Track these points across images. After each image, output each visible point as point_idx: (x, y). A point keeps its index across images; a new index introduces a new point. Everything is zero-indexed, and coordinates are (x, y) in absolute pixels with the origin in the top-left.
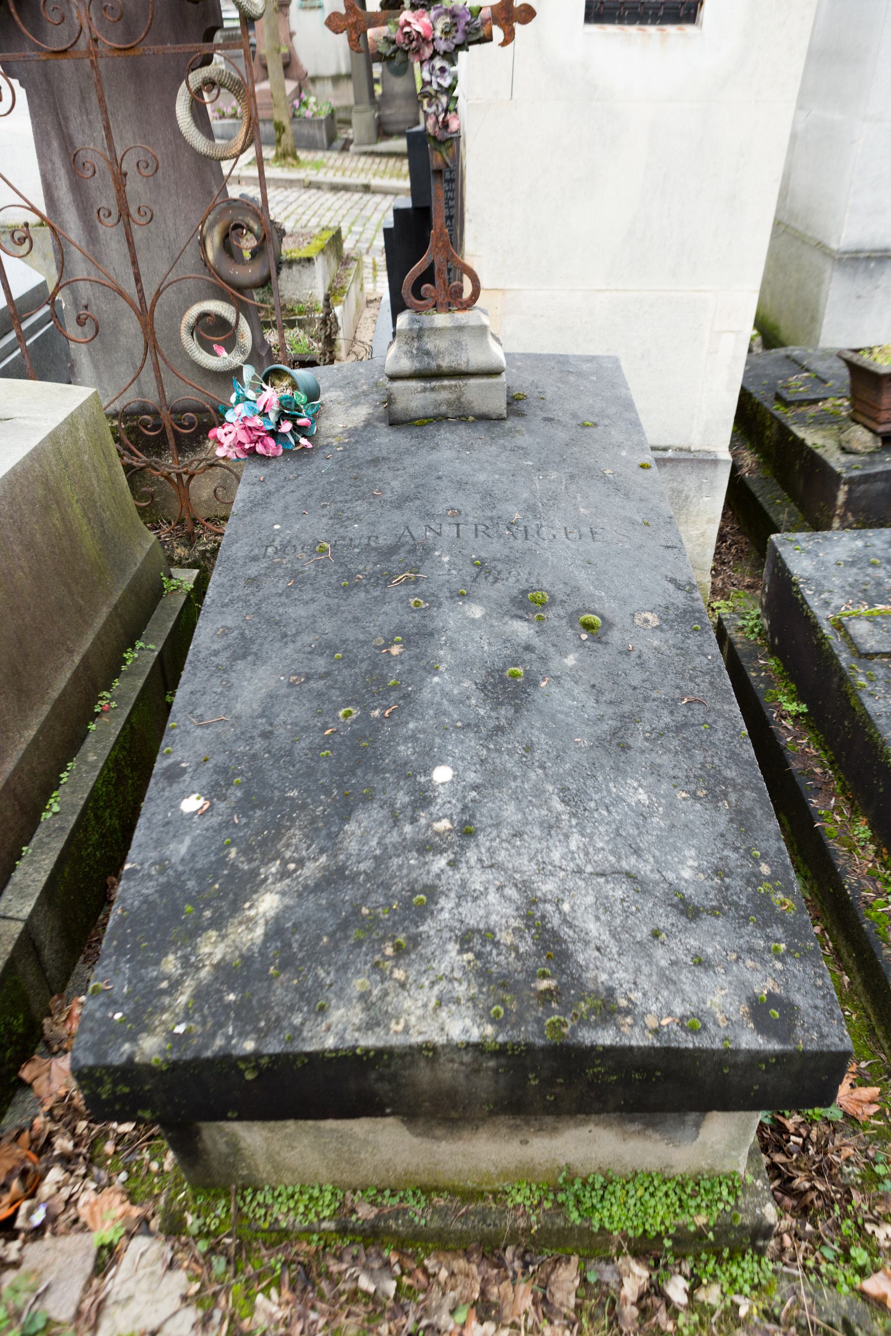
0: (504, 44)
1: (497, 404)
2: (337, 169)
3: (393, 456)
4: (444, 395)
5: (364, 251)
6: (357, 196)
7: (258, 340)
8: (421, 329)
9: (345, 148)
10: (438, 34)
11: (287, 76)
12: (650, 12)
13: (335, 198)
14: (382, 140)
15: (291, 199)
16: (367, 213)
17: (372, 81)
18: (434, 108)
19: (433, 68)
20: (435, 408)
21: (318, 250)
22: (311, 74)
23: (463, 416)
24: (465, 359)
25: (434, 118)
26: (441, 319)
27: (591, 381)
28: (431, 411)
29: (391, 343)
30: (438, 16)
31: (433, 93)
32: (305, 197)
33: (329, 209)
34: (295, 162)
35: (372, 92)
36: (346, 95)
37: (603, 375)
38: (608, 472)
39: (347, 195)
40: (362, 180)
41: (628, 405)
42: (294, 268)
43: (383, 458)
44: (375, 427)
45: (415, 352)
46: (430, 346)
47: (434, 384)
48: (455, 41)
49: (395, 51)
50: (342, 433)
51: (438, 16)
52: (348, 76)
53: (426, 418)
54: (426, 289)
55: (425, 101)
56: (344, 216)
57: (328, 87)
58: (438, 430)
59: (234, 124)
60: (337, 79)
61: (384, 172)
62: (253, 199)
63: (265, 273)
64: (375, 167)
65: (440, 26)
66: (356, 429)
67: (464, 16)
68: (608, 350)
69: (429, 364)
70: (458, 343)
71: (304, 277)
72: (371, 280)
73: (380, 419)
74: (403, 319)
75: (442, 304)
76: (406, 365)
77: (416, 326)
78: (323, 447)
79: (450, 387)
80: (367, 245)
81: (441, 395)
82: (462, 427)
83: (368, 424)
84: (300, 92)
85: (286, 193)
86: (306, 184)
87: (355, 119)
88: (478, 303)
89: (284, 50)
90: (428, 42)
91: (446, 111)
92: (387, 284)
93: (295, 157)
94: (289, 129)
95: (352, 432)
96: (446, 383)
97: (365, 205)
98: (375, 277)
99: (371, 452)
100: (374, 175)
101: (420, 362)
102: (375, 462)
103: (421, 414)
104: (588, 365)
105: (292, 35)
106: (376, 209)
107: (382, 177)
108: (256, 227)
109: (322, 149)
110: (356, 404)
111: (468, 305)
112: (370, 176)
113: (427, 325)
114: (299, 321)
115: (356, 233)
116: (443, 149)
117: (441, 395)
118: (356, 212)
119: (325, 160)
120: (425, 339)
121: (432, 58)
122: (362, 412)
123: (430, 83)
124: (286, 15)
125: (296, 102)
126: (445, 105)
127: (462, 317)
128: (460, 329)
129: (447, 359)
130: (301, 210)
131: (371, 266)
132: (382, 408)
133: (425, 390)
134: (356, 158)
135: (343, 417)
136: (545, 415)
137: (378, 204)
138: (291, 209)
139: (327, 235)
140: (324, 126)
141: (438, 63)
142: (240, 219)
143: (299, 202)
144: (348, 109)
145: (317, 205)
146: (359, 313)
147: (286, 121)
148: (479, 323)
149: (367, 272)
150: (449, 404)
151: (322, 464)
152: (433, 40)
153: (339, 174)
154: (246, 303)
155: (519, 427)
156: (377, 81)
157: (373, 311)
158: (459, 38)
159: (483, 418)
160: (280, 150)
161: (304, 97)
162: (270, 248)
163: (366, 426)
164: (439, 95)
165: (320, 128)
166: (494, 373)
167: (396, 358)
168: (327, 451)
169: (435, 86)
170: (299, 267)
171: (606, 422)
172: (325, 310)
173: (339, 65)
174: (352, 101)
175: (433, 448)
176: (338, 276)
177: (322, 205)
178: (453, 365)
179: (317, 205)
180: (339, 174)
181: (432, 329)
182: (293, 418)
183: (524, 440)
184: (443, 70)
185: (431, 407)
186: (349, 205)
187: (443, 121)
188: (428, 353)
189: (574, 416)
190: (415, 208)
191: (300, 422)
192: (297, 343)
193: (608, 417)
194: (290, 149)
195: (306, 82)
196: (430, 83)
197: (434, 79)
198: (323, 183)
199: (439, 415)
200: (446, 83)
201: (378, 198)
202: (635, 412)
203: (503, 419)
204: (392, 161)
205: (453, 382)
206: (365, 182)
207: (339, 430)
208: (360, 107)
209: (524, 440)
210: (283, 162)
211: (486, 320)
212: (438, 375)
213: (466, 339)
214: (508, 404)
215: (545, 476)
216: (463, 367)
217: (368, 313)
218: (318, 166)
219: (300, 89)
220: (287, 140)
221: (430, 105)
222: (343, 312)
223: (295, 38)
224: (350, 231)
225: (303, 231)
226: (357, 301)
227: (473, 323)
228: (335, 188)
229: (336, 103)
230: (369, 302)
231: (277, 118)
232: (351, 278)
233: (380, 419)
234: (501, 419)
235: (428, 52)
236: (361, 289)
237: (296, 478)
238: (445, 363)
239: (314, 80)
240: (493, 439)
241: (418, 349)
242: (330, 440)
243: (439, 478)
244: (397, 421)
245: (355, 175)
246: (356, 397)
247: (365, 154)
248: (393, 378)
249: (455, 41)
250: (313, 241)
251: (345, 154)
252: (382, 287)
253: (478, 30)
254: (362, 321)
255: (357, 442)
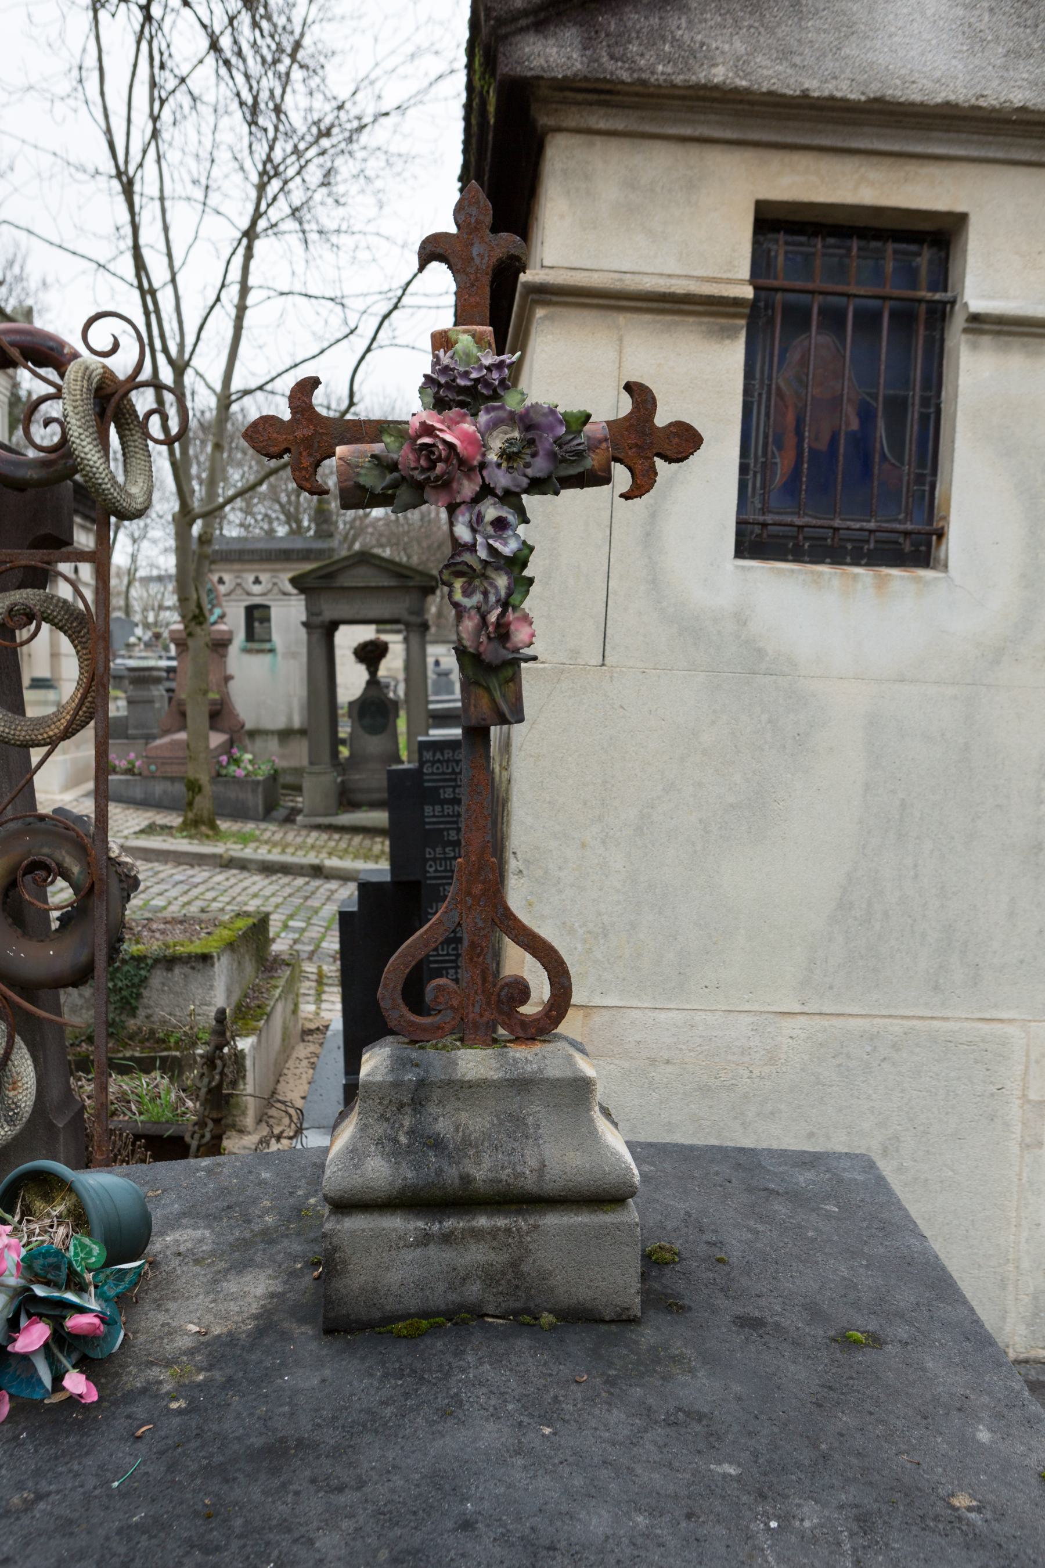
0: (626, 496)
1: (618, 1282)
2: (275, 845)
3: (330, 1437)
4: (477, 1254)
5: (304, 956)
6: (300, 881)
7: (54, 1094)
8: (421, 1083)
9: (289, 819)
10: (492, 457)
11: (213, 727)
12: (849, 546)
13: (267, 881)
14: (345, 811)
15: (196, 880)
16: (314, 903)
17: (336, 742)
18: (477, 598)
19: (480, 518)
20: (452, 1287)
21: (221, 944)
22: (249, 726)
23: (527, 1314)
24: (533, 1163)
25: (477, 619)
26: (474, 1063)
27: (829, 1216)
28: (439, 1297)
29: (342, 1116)
30: (494, 425)
31: (478, 566)
32: (220, 878)
33: (255, 896)
34: (210, 833)
35: (335, 753)
36: (299, 754)
37: (844, 1201)
38: (962, 1501)
39: (286, 880)
40: (312, 859)
41: (940, 1284)
42: (177, 971)
43: (300, 1443)
44: (285, 1336)
45: (403, 1140)
46: (443, 1126)
47: (450, 1223)
48: (529, 472)
49: (395, 485)
50: (191, 1352)
51: (494, 425)
52: (302, 732)
53: (425, 1315)
54: (439, 988)
55: (458, 584)
56: (277, 906)
57: (273, 744)
58: (459, 1354)
59: (127, 781)
60: (285, 735)
61: (346, 851)
62: (79, 819)
63: (83, 958)
64: (332, 844)
65: (497, 443)
66: (231, 1340)
67: (551, 428)
68: (811, 1135)
69: (439, 1172)
70: (517, 1121)
71: (193, 987)
72: (311, 999)
73: (300, 1313)
74: (374, 1063)
75: (476, 1026)
76: (378, 1171)
77: (410, 1076)
78: (131, 1397)
79: (494, 1233)
80: (310, 948)
81: (470, 1254)
82: (523, 1343)
83: (267, 1325)
84: (232, 747)
85: (190, 872)
86: (224, 862)
87: (307, 783)
88: (562, 1029)
89: (213, 696)
90: (472, 469)
91: (505, 605)
92: (339, 1006)
93: (213, 827)
94: (208, 788)
95: (218, 1350)
96: (482, 1221)
97: (313, 893)
98: (319, 994)
99: (265, 1420)
100: (330, 854)
101: (417, 1166)
102: (276, 1454)
103: (412, 1303)
104: (810, 1175)
105: (228, 679)
106: (328, 899)
107: (341, 858)
108: (76, 870)
109: (255, 819)
110: (240, 1267)
111: (542, 1028)
112: (323, 855)
113: (437, 1074)
114: (164, 1060)
115: (294, 930)
116: (494, 683)
117: (470, 1254)
118: (297, 901)
119: (257, 832)
120: (433, 1109)
121: (477, 499)
122: (255, 1288)
123: (472, 548)
124: (224, 656)
125: (224, 759)
126: (503, 593)
127: (526, 1057)
128: (522, 1085)
129: (487, 1162)
130: (209, 895)
131: (314, 977)
132: (307, 1281)
133: (425, 1240)
134: (304, 833)
135: (202, 1301)
136: (739, 1310)
137: (333, 892)
138: (195, 892)
139: (242, 924)
140: (260, 789)
141: (491, 511)
142: (44, 852)
143: (209, 885)
144: (298, 771)
145: (237, 889)
146: (286, 1050)
147: (204, 779)
148: (569, 1074)
149: (307, 987)
150: (489, 1276)
151: (122, 1459)
152: (483, 465)
153: (277, 850)
154: (40, 1020)
155: (677, 1347)
156: (343, 742)
157: (312, 1048)
158: (540, 466)
159: (579, 1317)
160: (190, 815)
161: (236, 752)
162: (99, 910)
163: (260, 1332)
164: (490, 572)
165: (254, 791)
166: (608, 1197)
167: (354, 1153)
168: (139, 1410)
169: (483, 553)
170: (186, 970)
171: (902, 1332)
172: (215, 1040)
173: (290, 718)
174: (305, 762)
175: (445, 1414)
176: (256, 989)
177: (245, 889)
178: (503, 1175)
179: (237, 889)
180: (278, 849)
181: (450, 1083)
182: (56, 1312)
183: (699, 1388)
184: (500, 524)
185: (441, 1287)
186: (288, 890)
187: (498, 624)
188: (437, 1144)
189: (815, 1313)
190: (396, 883)
191: (76, 1322)
192: (153, 1100)
193: (900, 1315)
194: (205, 814)
195: (240, 736)
196: (472, 548)
197: (480, 539)
198: (250, 861)
199: (462, 1307)
200: (508, 548)
201: (333, 885)
202: (965, 1302)
203: (633, 1321)
204: (357, 839)
205: (501, 1222)
206: (316, 861)
207: (184, 1342)
208: (316, 769)
209: (699, 1388)
210: (193, 831)
211: (587, 1068)
212: (464, 1200)
213: (536, 1111)
214: (644, 1276)
215: (785, 1519)
216: (529, 1183)
217: (302, 1051)
218: (244, 839)
219: (231, 743)
220: (203, 803)
221: (466, 593)
222: (255, 1048)
223: (232, 684)
224: (286, 927)
225: (204, 916)
226: (285, 1029)
227: (554, 1071)
228: (268, 869)
229: (281, 764)
230: (307, 1033)
231: (191, 775)
232: (278, 991)
233: (300, 1313)
234: (626, 1320)
235: (468, 489)
236: (295, 1011)
237: (28, 1506)
238: (482, 1170)
239: (253, 734)
240: (611, 1382)
241: (411, 1133)
242: (155, 1372)
243: (467, 1525)
244: (345, 1321)
245: (300, 853)
246: (245, 1244)
247: (318, 827)
248: (344, 1205)
249: (529, 472)
250: (217, 931)
251: (289, 826)
252: (331, 1011)
253: (580, 455)
254: (290, 1064)
255: (230, 1382)
